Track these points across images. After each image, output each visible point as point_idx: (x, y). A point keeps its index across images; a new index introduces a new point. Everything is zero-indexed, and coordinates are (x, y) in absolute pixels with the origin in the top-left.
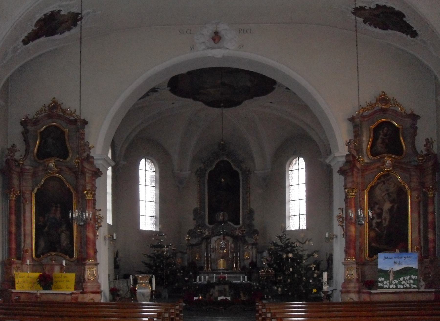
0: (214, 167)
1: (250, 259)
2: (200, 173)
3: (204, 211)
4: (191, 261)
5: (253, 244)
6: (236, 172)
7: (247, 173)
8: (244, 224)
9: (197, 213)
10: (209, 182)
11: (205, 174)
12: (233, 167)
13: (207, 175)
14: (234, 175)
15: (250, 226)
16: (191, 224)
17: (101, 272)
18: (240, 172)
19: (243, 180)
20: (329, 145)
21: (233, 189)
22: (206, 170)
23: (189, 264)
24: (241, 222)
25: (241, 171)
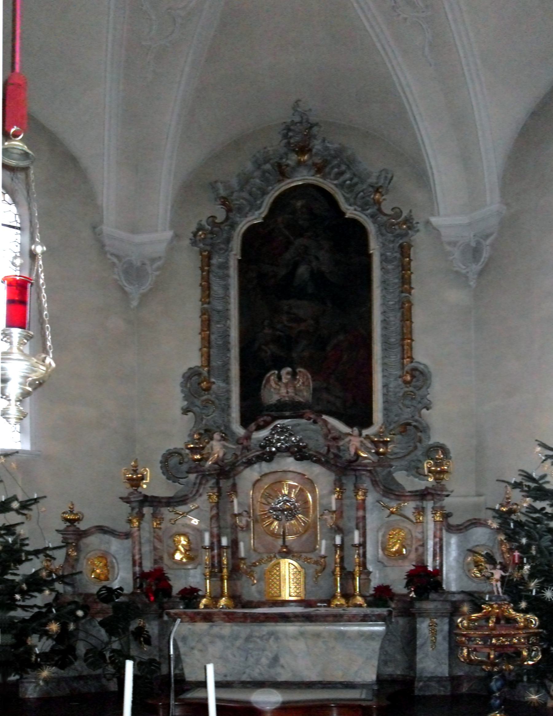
0: (264, 210)
1: (413, 556)
2: (208, 241)
3: (227, 380)
4: (148, 566)
5: (423, 495)
6: (355, 224)
7: (402, 230)
8: (387, 421)
9: (196, 385)
10: (244, 266)
11: (228, 241)
12: (344, 206)
13: (236, 244)
14: (352, 237)
15: (412, 429)
16: (177, 430)
17: (546, 522)
18: (371, 228)
19: (385, 259)
20: (202, 325)
21: (348, 289)
22: (233, 226)
23: (141, 577)
24: (378, 416)
25: (374, 222)
